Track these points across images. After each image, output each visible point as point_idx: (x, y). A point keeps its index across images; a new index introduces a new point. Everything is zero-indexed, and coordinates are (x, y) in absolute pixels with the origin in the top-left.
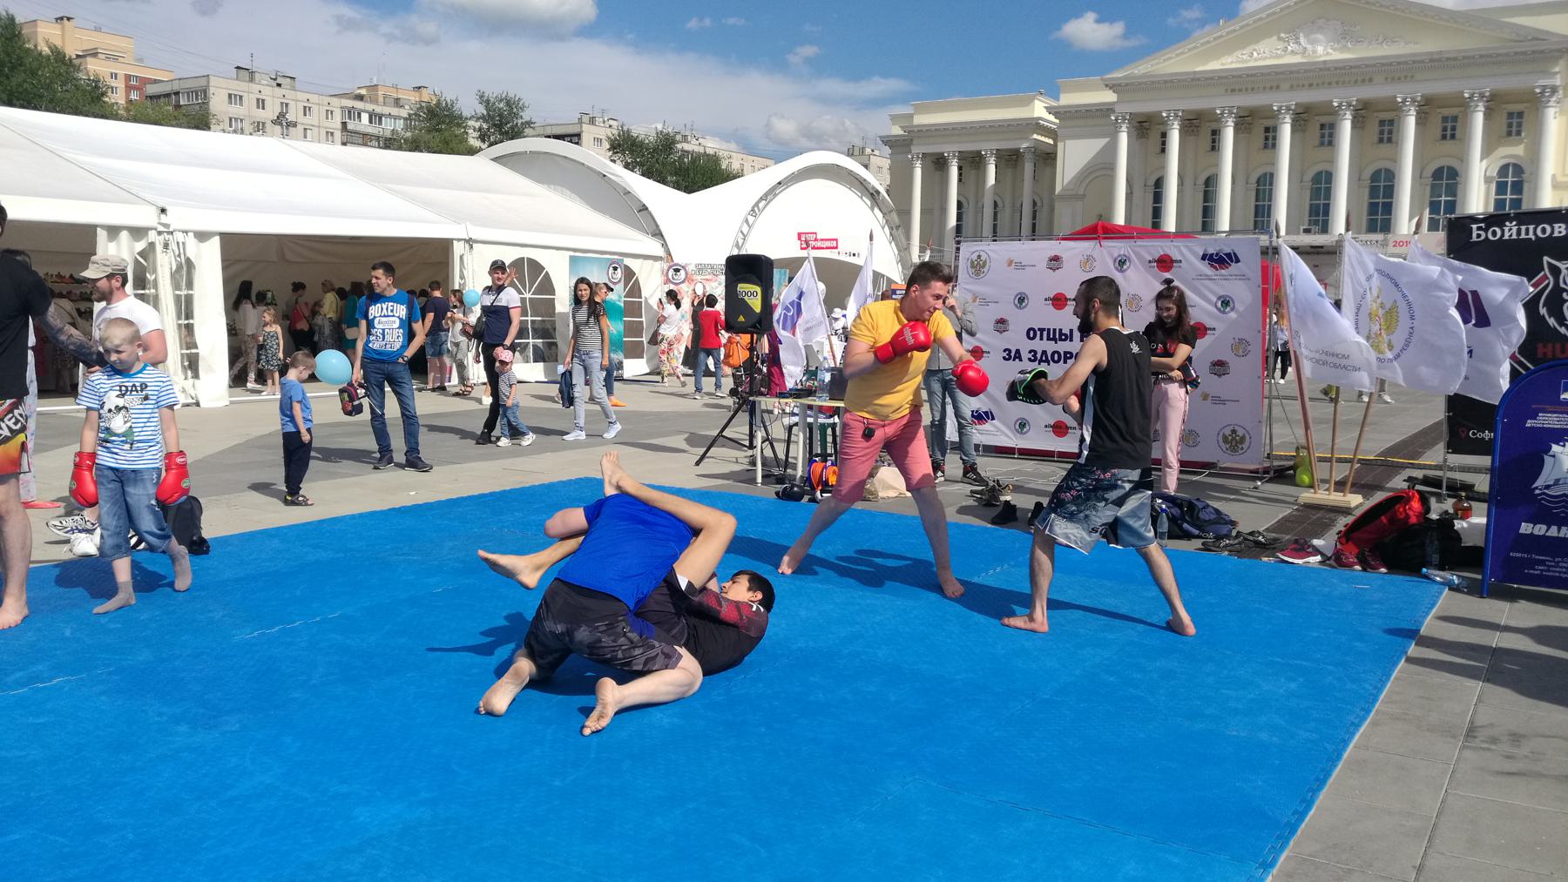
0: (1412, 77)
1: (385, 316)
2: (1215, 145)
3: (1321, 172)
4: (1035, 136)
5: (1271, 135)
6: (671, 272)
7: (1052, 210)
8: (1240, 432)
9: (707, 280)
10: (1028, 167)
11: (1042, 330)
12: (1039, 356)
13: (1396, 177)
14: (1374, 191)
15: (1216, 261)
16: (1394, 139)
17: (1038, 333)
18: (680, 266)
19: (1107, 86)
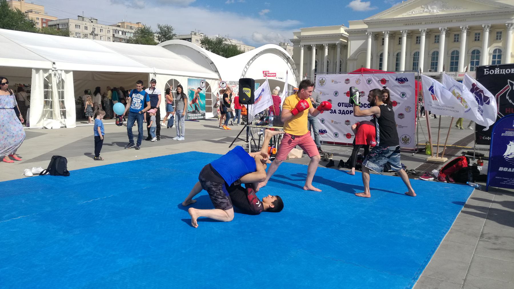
0: (465, 20)
1: (137, 98)
2: (400, 42)
3: (435, 52)
4: (341, 39)
5: (418, 39)
6: (221, 84)
7: (346, 64)
8: (408, 137)
9: (233, 86)
10: (339, 50)
11: (343, 103)
12: (342, 112)
13: (460, 53)
14: (452, 58)
15: (400, 81)
16: (480, 39)
17: (342, 104)
18: (224, 82)
19: (365, 23)
